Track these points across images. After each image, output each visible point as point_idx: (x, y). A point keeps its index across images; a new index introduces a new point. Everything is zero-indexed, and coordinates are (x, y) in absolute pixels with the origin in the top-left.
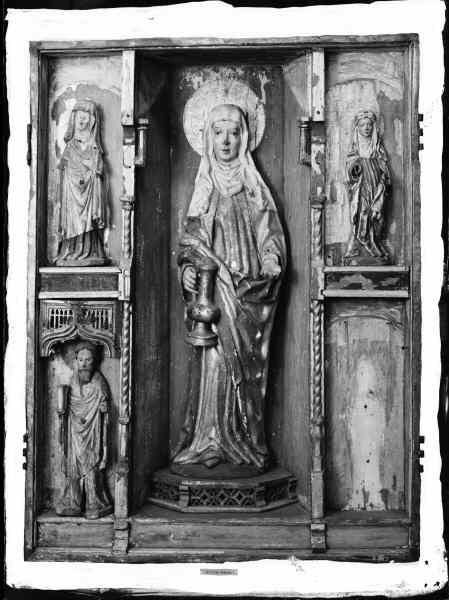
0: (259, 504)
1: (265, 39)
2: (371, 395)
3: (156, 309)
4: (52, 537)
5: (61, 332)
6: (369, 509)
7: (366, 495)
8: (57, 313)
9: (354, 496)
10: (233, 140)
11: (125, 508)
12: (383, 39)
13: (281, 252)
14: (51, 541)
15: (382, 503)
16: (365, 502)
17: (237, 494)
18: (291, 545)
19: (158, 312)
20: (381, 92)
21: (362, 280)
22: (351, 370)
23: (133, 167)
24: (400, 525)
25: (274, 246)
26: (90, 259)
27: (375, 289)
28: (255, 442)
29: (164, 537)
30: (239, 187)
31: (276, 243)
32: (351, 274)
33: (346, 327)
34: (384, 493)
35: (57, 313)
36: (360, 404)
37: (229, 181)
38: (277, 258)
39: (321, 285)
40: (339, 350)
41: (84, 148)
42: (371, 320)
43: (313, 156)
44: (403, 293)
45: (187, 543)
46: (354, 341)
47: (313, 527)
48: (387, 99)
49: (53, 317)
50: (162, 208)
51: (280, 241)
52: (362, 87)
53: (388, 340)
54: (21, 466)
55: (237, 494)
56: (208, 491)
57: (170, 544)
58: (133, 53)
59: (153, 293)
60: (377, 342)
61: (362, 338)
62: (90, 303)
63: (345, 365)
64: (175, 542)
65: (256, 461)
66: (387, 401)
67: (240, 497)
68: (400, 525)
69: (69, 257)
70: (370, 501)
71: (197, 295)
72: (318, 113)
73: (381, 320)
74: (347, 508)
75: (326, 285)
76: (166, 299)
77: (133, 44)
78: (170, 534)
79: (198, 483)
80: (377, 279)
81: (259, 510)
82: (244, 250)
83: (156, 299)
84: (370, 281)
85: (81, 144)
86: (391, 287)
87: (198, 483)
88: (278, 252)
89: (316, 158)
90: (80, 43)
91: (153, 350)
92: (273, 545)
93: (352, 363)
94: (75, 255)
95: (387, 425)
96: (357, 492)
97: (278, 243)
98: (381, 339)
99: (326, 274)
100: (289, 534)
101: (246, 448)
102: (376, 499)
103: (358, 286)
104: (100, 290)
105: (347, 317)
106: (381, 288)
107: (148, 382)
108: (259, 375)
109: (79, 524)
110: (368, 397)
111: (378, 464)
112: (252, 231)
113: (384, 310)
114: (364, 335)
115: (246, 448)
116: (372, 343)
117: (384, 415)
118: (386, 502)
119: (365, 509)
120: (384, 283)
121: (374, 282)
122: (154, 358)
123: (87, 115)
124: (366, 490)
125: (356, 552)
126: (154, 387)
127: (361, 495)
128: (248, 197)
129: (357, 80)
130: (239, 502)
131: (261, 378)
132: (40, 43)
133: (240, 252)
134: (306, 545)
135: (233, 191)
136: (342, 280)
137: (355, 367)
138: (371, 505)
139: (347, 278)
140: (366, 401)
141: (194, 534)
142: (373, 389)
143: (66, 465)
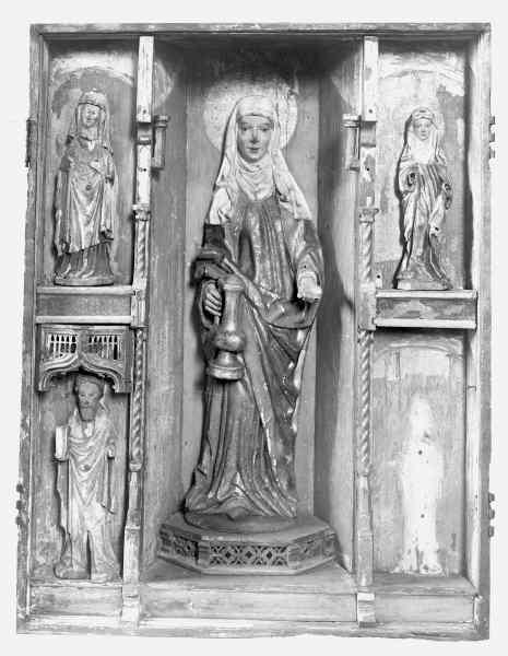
0: (291, 564)
1: (310, 26)
2: (427, 440)
3: (169, 330)
4: (48, 603)
5: (62, 361)
6: (423, 572)
7: (419, 555)
8: (63, 340)
9: (405, 556)
11: (136, 571)
12: (449, 28)
13: (319, 269)
14: (48, 607)
15: (439, 566)
16: (418, 565)
17: (266, 552)
18: (332, 617)
19: (172, 333)
20: (441, 86)
21: (420, 307)
22: (404, 410)
23: (148, 169)
24: (463, 594)
25: (311, 261)
26: (95, 278)
27: (436, 318)
28: (285, 487)
29: (180, 605)
31: (312, 258)
32: (407, 300)
33: (398, 358)
34: (441, 553)
35: (63, 340)
36: (414, 444)
37: (257, 185)
38: (315, 277)
39: (373, 312)
40: (389, 386)
41: (91, 146)
42: (427, 351)
43: (363, 160)
44: (468, 324)
45: (209, 613)
46: (407, 375)
47: (361, 596)
48: (450, 95)
49: (52, 345)
50: (178, 214)
51: (318, 255)
52: (419, 80)
53: (447, 374)
54: (14, 520)
55: (266, 552)
56: (233, 547)
57: (187, 613)
58: (151, 39)
59: (167, 314)
60: (434, 378)
61: (417, 372)
62: (96, 328)
63: (395, 403)
64: (195, 612)
65: (263, 400)
66: (445, 446)
67: (269, 555)
68: (463, 594)
69: (71, 275)
70: (424, 562)
71: (221, 317)
72: (371, 111)
73: (439, 352)
74: (397, 570)
75: (378, 313)
76: (180, 318)
77: (152, 28)
78: (189, 601)
79: (221, 538)
80: (439, 305)
81: (292, 572)
83: (170, 319)
85: (89, 143)
86: (455, 316)
87: (221, 538)
88: (316, 269)
89: (366, 163)
90: (89, 26)
91: (165, 378)
92: (311, 617)
93: (404, 402)
94: (79, 273)
95: (445, 474)
96: (410, 551)
97: (316, 258)
98: (440, 373)
100: (328, 603)
101: (275, 495)
102: (432, 561)
104: (109, 314)
105: (399, 348)
106: (442, 317)
107: (160, 418)
108: (290, 411)
109: (80, 588)
110: (423, 441)
111: (434, 520)
112: (285, 244)
113: (442, 342)
114: (418, 370)
115: (275, 495)
116: (429, 378)
117: (441, 461)
118: (443, 565)
119: (418, 571)
120: (448, 312)
121: (435, 310)
122: (167, 388)
123: (96, 109)
124: (420, 549)
125: (413, 628)
126: (166, 422)
127: (414, 554)
129: (414, 72)
130: (269, 561)
131: (292, 414)
132: (41, 26)
134: (351, 617)
136: (397, 306)
137: (409, 404)
138: (426, 568)
139: (404, 305)
140: (423, 446)
141: (217, 602)
142: (429, 432)
143: (59, 630)
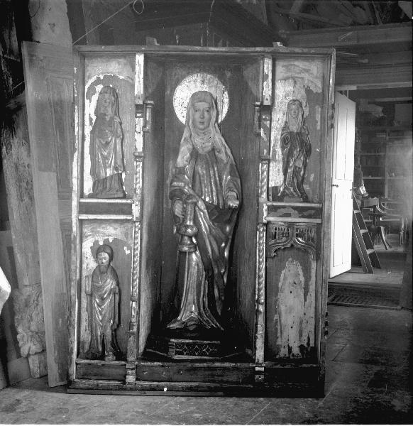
10: (206, 113)
27: (300, 217)
30: (210, 148)
75: (268, 213)
82: (214, 189)
84: (296, 212)
99: (268, 207)
103: (288, 215)
128: (217, 154)
133: (212, 191)
135: (206, 150)
139: (282, 210)
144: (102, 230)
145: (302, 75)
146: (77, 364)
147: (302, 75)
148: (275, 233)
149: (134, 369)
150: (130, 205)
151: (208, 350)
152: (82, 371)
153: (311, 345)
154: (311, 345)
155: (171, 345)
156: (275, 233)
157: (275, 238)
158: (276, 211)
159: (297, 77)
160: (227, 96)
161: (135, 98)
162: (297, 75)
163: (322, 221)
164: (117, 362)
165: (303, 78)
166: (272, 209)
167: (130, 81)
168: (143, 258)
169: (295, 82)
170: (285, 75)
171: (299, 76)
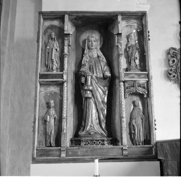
27: (139, 78)
103: (133, 77)
139: (130, 75)
144: (49, 89)
145: (134, 24)
146: (37, 150)
147: (134, 24)
148: (128, 86)
149: (65, 150)
150: (62, 75)
151: (100, 143)
152: (39, 154)
153: (148, 139)
154: (148, 139)
155: (82, 141)
156: (128, 86)
157: (128, 88)
158: (128, 76)
159: (132, 25)
160: (102, 38)
161: (68, 40)
162: (131, 24)
163: (148, 79)
164: (57, 148)
165: (134, 25)
166: (126, 75)
167: (62, 28)
168: (85, 115)
169: (131, 27)
170: (126, 25)
171: (133, 24)
